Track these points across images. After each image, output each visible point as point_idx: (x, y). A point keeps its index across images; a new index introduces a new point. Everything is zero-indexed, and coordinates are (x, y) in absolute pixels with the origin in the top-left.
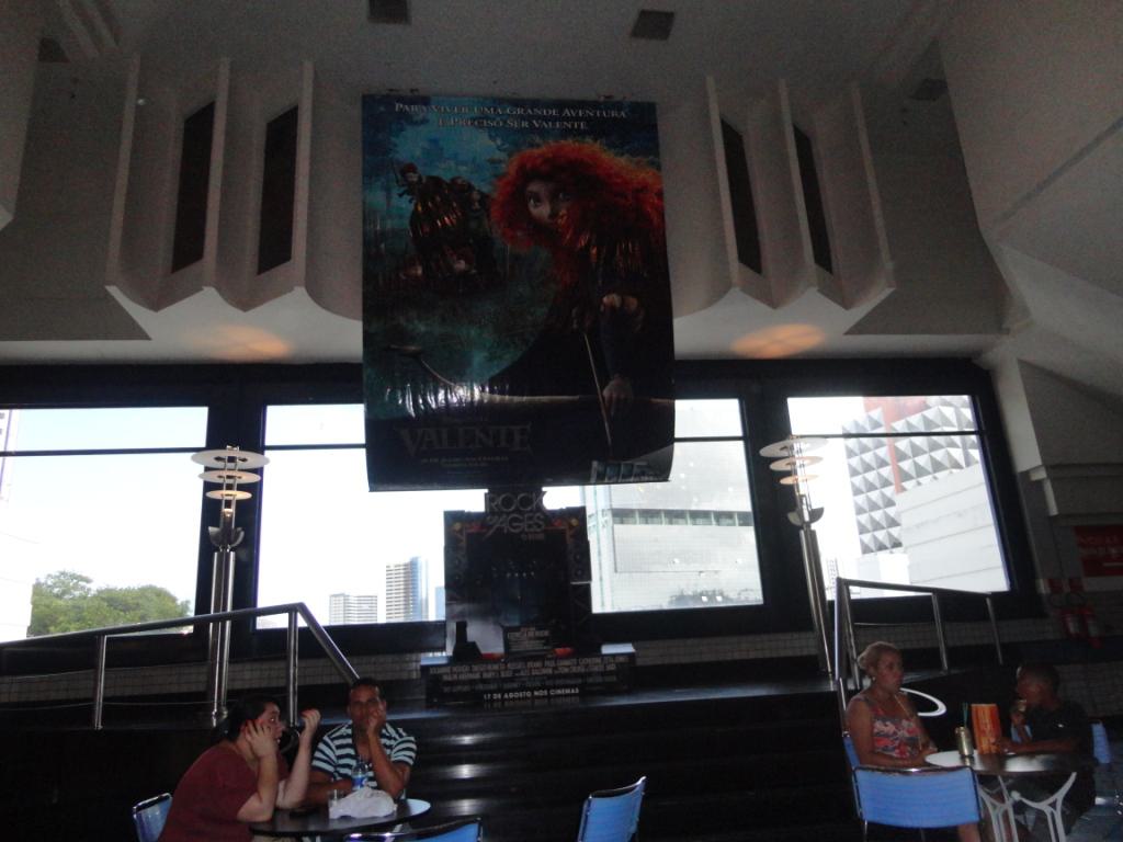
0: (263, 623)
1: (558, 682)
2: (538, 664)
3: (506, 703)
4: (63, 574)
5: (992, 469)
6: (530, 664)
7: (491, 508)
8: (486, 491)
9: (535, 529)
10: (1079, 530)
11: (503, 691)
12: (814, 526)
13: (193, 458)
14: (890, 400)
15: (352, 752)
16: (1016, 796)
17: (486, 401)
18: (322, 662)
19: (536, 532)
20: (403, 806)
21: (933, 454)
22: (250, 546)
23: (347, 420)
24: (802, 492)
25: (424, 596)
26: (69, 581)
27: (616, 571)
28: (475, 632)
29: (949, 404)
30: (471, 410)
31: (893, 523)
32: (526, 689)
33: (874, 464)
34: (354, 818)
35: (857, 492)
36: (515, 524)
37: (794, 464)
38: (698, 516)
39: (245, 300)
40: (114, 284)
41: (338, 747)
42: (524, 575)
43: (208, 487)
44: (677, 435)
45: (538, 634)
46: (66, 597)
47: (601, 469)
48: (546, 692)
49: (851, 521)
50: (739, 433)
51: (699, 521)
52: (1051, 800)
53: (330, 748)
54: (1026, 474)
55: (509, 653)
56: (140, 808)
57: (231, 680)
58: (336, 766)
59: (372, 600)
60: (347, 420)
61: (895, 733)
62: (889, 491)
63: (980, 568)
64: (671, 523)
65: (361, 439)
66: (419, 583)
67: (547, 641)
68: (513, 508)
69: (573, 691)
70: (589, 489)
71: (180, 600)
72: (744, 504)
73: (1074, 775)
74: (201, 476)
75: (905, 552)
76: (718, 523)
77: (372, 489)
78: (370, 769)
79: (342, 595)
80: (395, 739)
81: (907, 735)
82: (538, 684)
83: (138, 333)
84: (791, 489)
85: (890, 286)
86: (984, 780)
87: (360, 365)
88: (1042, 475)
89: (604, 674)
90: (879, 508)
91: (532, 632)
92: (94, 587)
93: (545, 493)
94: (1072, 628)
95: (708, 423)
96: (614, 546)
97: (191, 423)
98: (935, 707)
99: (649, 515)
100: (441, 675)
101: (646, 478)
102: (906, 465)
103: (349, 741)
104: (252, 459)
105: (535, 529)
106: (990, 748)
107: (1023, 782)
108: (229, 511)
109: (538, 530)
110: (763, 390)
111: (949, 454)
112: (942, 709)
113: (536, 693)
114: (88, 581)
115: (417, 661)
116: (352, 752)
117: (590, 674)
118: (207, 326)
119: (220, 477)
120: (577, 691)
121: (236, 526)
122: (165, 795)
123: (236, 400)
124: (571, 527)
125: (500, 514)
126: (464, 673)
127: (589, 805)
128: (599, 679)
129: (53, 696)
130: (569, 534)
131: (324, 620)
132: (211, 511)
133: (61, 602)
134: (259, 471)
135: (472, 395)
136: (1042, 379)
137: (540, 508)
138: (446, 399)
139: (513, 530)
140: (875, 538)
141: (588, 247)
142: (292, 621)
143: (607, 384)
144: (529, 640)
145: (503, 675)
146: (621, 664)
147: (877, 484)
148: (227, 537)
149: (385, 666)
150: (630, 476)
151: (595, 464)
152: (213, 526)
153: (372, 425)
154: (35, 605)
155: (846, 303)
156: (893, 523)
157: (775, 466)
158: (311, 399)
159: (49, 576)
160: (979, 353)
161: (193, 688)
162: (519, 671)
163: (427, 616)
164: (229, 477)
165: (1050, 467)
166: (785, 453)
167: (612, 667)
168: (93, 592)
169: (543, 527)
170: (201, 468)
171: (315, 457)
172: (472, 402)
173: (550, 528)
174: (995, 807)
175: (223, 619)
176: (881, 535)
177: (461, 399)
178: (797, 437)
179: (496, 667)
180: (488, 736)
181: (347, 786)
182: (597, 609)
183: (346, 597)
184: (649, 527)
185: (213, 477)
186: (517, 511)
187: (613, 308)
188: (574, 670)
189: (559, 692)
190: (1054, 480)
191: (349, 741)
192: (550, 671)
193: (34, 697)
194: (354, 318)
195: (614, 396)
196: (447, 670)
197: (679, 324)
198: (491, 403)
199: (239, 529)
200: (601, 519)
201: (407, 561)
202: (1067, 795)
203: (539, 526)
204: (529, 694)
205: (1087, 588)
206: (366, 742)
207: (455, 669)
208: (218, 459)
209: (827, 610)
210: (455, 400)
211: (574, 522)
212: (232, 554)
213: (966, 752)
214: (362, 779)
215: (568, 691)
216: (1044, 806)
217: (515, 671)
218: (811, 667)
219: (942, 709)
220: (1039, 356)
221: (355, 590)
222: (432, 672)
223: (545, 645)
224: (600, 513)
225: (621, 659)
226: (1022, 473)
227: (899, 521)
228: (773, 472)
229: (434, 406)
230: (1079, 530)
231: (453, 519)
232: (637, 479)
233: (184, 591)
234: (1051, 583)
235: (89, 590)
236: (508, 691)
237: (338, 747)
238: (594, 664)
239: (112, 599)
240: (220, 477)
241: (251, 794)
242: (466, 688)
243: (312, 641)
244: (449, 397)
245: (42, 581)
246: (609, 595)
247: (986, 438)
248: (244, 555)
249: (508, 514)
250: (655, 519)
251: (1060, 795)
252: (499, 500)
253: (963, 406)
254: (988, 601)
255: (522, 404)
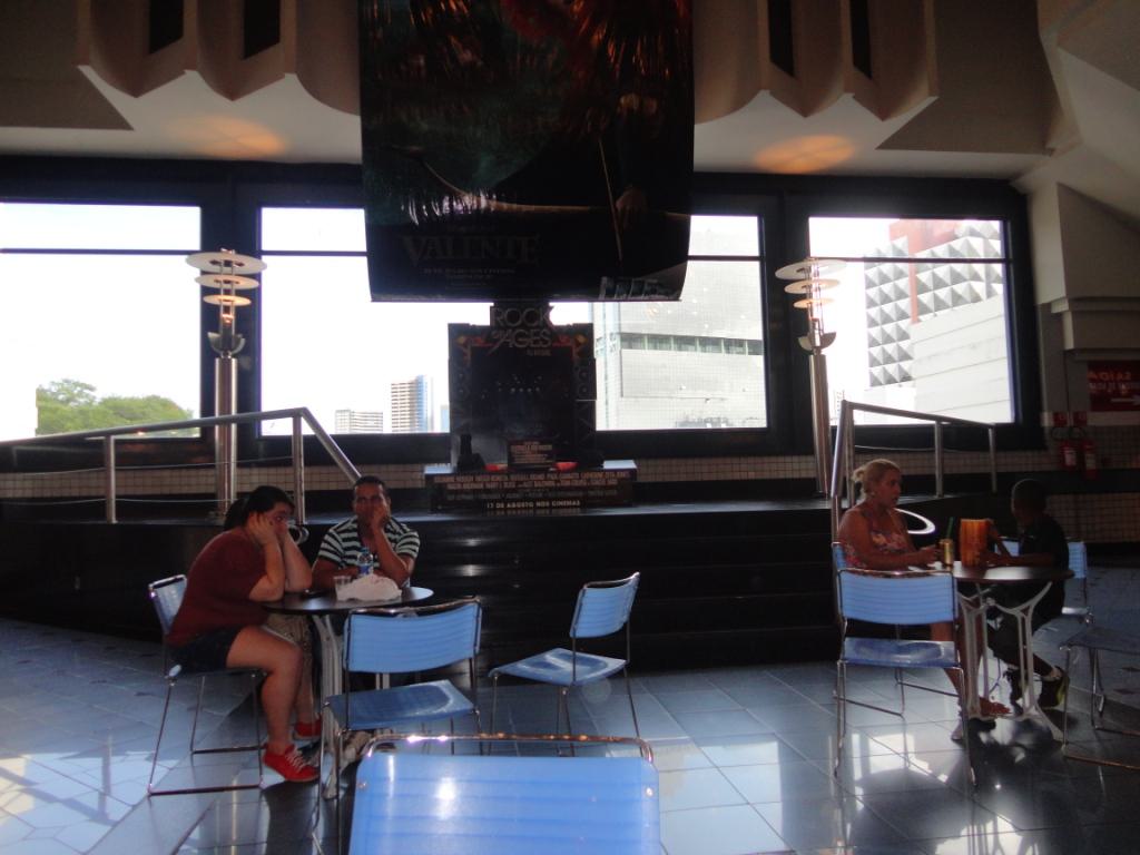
0: (271, 428)
1: (560, 494)
2: (541, 477)
3: (509, 512)
4: (67, 381)
5: (1014, 302)
6: (533, 477)
7: (497, 322)
8: (492, 304)
9: (541, 344)
10: (1095, 366)
11: (506, 501)
12: (824, 351)
13: (188, 261)
14: (917, 224)
15: (357, 544)
16: (991, 602)
17: (492, 209)
18: (332, 469)
19: (541, 348)
20: (406, 593)
21: (955, 287)
22: (252, 352)
23: (347, 226)
24: (815, 316)
25: (429, 415)
26: (73, 389)
27: (622, 396)
28: (477, 444)
29: (973, 233)
30: (478, 216)
31: (905, 356)
32: (528, 500)
33: (896, 356)
34: (361, 601)
35: (872, 323)
36: (520, 340)
37: (810, 287)
38: (709, 343)
39: (232, 85)
40: (87, 64)
41: (345, 540)
42: (529, 390)
43: (206, 291)
44: (691, 253)
45: (542, 448)
46: (72, 404)
47: (611, 285)
48: (548, 504)
49: (862, 352)
50: (756, 253)
51: (709, 348)
52: (1024, 606)
53: (336, 539)
54: (1048, 306)
55: (514, 467)
56: (156, 587)
57: (240, 483)
58: (342, 557)
59: (378, 416)
60: (347, 226)
61: (885, 545)
62: (904, 324)
63: (987, 398)
64: (680, 349)
65: (362, 246)
66: (425, 394)
67: (549, 455)
68: (519, 322)
69: (574, 503)
70: (598, 306)
71: (184, 407)
72: (755, 331)
73: (1050, 584)
74: (197, 280)
75: (914, 386)
76: (728, 351)
77: (375, 299)
78: (375, 560)
79: (347, 411)
80: (400, 534)
81: (896, 547)
82: (541, 495)
83: (119, 123)
84: (805, 312)
85: (931, 95)
86: (963, 586)
87: (359, 166)
88: (1063, 307)
89: (606, 487)
90: (894, 361)
91: (535, 446)
92: (99, 395)
93: (551, 308)
94: (1070, 459)
95: (723, 238)
96: (621, 371)
97: (182, 223)
98: (923, 526)
99: (658, 341)
100: (446, 484)
101: (657, 296)
102: (925, 298)
103: (355, 535)
104: (249, 264)
105: (541, 344)
106: (974, 561)
107: (1007, 592)
108: (229, 317)
109: (545, 346)
110: (784, 206)
111: (971, 288)
112: (930, 528)
113: (538, 504)
114: (92, 389)
115: (422, 471)
116: (357, 544)
117: (592, 488)
118: (185, 115)
119: (217, 281)
120: (578, 503)
121: (237, 332)
122: (179, 576)
123: (230, 199)
124: (578, 344)
125: (506, 328)
126: (468, 483)
127: (584, 593)
128: (600, 493)
129: (66, 493)
130: (575, 351)
131: (331, 428)
132: (210, 316)
133: (64, 408)
134: (257, 277)
135: (479, 203)
136: (1087, 212)
137: (547, 324)
138: (451, 206)
139: (517, 345)
140: (885, 371)
141: (603, 44)
142: (297, 426)
143: (619, 197)
144: (531, 453)
145: (506, 486)
146: (623, 479)
147: (894, 317)
148: (227, 344)
149: (393, 476)
150: (641, 294)
151: (604, 280)
152: (212, 331)
153: (373, 231)
154: (41, 410)
155: (883, 113)
156: (905, 356)
157: (790, 289)
158: (308, 202)
159: (53, 383)
160: (1018, 175)
161: (202, 490)
162: (522, 483)
163: (432, 427)
164: (227, 282)
165: (1075, 300)
166: (801, 275)
167: (613, 482)
168: (98, 400)
169: (549, 344)
170: (196, 272)
171: (315, 255)
172: (478, 209)
173: (555, 344)
174: (969, 610)
175: (225, 423)
176: (892, 368)
177: (466, 206)
178: (816, 259)
179: (499, 478)
180: (491, 540)
181: (354, 573)
182: (601, 425)
183: (352, 414)
184: (658, 352)
185: (210, 282)
186: (522, 326)
187: (630, 110)
188: (576, 483)
189: (561, 503)
190: (1076, 314)
191: (355, 535)
192: (552, 484)
193: (47, 494)
194: (355, 114)
195: (628, 208)
196: (452, 479)
197: (700, 130)
198: (498, 212)
199: (240, 336)
200: (610, 343)
201: (413, 379)
202: (1039, 603)
203: (546, 342)
204: (531, 505)
205: (1090, 423)
206: (371, 536)
207: (459, 479)
208: (214, 263)
209: (830, 435)
210: (460, 207)
211: (581, 339)
212: (234, 361)
213: (948, 561)
214: (368, 567)
215: (569, 503)
216: (1016, 611)
217: (517, 483)
218: (810, 488)
219: (930, 528)
220: (1086, 182)
221: (361, 406)
222: (437, 480)
223: (548, 458)
224: (608, 337)
225: (623, 475)
226: (1044, 305)
227: (910, 353)
228: (787, 294)
229: (438, 213)
230: (1095, 366)
231: (458, 332)
232: (647, 297)
233: (191, 404)
234: (1056, 416)
235: (94, 397)
236: (511, 501)
237: (345, 540)
238: (595, 478)
239: (115, 406)
240: (217, 281)
241: (261, 577)
242: (470, 497)
243: (316, 450)
244: (455, 204)
245: (46, 387)
246: (612, 414)
247: (1011, 267)
248: (246, 362)
249: (514, 329)
250: (664, 345)
251: (1033, 603)
252: (505, 315)
253: (992, 238)
254: (990, 430)
255: (528, 213)
